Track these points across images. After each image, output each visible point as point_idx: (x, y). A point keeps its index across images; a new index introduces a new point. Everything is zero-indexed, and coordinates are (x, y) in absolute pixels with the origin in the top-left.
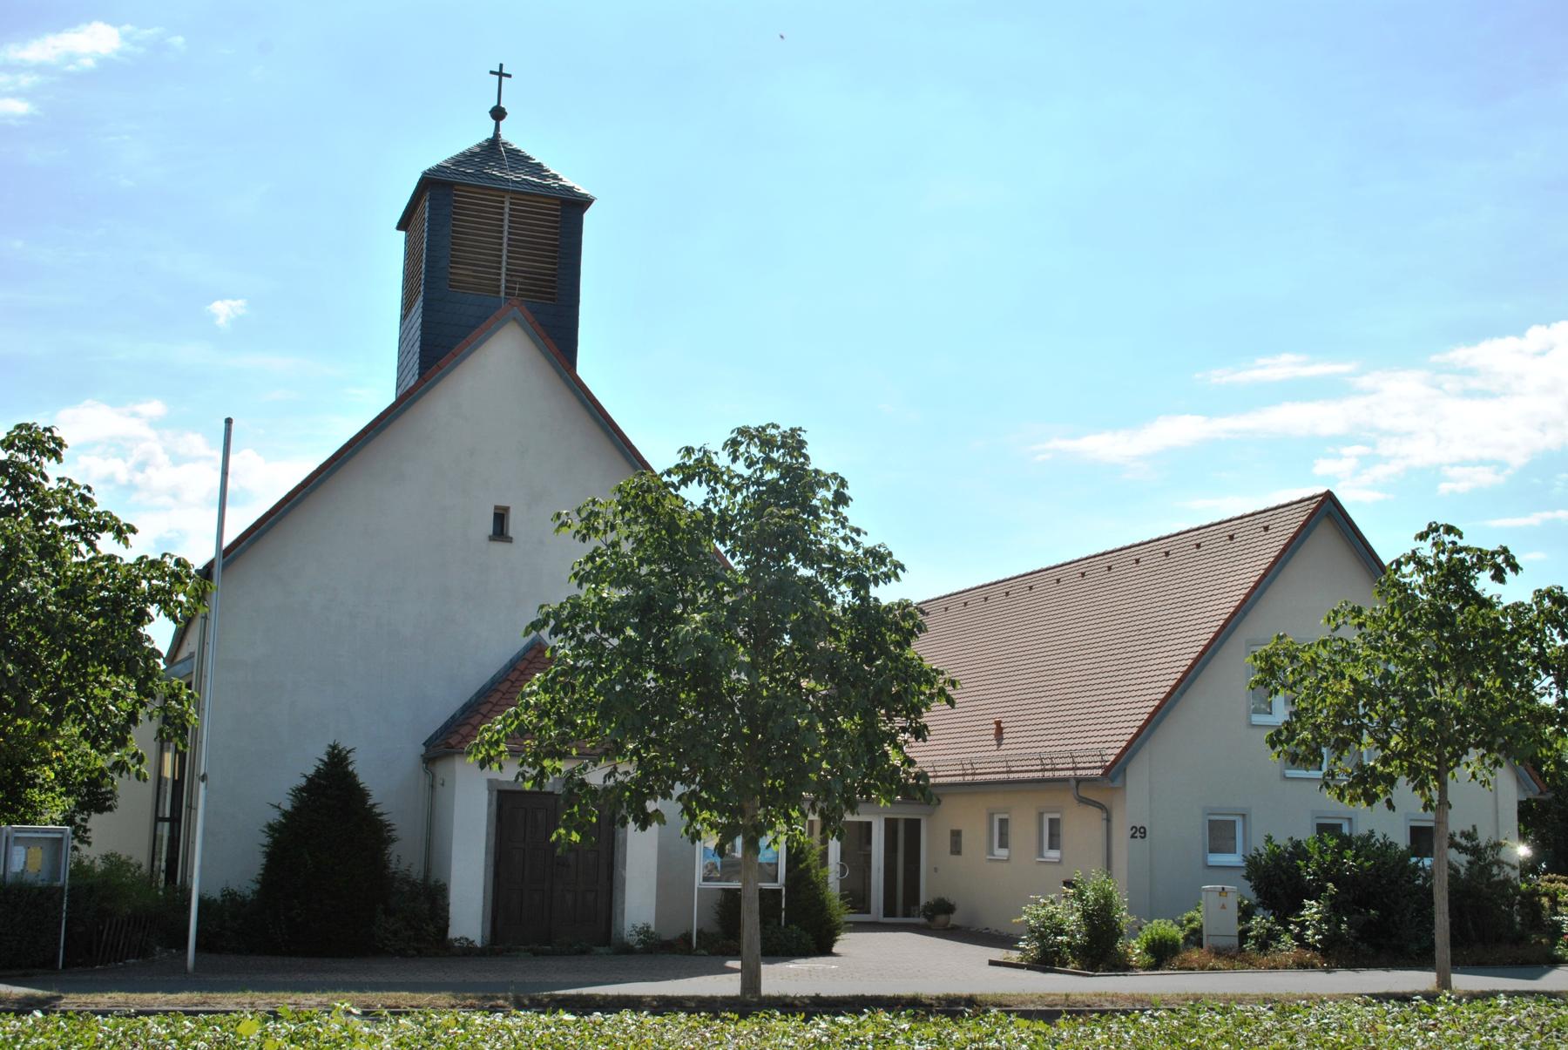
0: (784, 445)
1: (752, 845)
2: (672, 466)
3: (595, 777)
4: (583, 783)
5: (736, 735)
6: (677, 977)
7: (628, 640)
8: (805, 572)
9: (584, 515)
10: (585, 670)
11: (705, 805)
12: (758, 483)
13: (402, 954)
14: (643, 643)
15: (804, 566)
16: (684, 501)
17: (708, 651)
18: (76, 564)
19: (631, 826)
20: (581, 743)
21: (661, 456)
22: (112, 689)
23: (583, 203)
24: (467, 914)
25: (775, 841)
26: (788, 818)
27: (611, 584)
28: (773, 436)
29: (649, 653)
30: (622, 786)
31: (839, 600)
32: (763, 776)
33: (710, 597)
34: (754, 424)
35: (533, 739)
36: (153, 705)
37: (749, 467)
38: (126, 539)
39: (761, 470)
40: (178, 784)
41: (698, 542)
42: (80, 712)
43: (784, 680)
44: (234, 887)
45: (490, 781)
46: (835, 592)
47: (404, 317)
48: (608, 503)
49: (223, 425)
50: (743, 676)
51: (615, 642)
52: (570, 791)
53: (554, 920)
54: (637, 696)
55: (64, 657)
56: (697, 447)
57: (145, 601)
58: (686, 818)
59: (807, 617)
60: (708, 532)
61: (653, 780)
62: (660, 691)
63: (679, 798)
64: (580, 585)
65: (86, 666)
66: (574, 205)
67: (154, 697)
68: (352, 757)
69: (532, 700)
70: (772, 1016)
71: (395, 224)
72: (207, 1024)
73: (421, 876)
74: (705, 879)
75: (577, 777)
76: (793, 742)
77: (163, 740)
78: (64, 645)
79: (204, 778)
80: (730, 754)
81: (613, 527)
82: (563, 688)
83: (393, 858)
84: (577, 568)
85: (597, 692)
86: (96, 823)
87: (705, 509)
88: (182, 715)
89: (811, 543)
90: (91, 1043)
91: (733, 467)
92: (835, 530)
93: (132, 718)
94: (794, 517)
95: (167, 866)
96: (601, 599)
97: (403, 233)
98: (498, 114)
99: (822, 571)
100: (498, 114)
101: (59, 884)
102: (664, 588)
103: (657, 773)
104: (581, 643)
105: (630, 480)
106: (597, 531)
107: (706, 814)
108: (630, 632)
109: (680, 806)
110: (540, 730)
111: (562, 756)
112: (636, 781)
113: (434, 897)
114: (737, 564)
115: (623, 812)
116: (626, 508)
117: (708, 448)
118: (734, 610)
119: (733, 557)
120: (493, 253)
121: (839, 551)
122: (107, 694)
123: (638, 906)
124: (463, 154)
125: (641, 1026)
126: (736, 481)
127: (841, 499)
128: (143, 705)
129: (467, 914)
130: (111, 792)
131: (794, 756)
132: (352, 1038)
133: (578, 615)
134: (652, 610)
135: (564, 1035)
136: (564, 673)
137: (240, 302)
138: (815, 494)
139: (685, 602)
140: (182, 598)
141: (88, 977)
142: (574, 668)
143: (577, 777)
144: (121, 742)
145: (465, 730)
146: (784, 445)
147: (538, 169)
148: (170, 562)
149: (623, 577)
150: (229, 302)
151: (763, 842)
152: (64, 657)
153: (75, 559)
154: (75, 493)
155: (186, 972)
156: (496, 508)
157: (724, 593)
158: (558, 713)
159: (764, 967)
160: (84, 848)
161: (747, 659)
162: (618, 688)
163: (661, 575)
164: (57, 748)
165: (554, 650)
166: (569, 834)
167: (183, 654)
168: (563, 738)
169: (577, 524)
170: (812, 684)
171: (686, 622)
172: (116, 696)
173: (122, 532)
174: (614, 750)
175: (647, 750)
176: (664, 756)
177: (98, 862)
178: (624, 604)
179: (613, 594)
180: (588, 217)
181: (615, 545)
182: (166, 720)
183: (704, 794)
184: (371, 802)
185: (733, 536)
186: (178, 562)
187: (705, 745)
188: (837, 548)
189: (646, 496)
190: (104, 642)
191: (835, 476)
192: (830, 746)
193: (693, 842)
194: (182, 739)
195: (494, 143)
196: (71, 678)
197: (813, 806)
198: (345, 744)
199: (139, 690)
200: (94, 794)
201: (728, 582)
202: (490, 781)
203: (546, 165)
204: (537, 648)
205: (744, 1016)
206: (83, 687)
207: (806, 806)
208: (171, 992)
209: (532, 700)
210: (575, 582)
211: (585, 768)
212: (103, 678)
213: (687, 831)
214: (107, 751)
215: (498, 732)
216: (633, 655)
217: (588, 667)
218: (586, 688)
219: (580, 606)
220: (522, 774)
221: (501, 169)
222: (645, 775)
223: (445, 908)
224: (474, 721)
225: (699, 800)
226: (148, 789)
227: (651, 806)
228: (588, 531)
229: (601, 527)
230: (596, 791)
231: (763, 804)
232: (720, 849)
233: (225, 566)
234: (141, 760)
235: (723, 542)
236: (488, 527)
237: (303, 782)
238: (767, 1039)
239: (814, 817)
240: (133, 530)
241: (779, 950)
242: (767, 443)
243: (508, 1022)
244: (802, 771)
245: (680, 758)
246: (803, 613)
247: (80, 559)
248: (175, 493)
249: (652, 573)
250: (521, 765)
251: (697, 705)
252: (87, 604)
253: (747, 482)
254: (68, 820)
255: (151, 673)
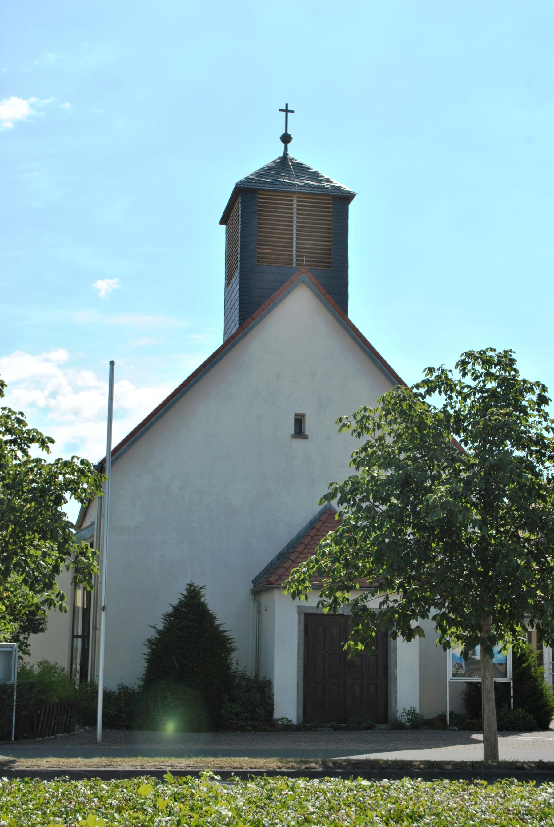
0: (499, 363)
1: (488, 651)
2: (419, 381)
3: (374, 603)
4: (365, 609)
5: (473, 572)
6: (437, 746)
7: (392, 505)
8: (519, 453)
9: (358, 418)
10: (363, 529)
11: (452, 623)
12: (481, 391)
13: (242, 729)
14: (404, 509)
15: (518, 449)
16: (429, 406)
17: (451, 513)
18: (16, 465)
19: (400, 638)
20: (362, 580)
21: (411, 375)
22: (41, 550)
23: (348, 197)
24: (287, 703)
25: (504, 648)
26: (513, 631)
27: (380, 467)
28: (491, 357)
29: (408, 516)
30: (392, 610)
31: (545, 472)
32: (494, 602)
33: (450, 474)
34: (477, 348)
35: (328, 577)
36: (69, 560)
37: (475, 380)
38: (47, 447)
39: (484, 381)
40: (86, 611)
41: (441, 434)
42: (20, 567)
43: (507, 532)
44: (126, 683)
45: (299, 607)
46: (533, 431)
47: (227, 285)
48: (376, 409)
49: (108, 366)
50: (477, 530)
51: (384, 508)
52: (356, 614)
53: (347, 703)
54: (401, 546)
55: (10, 529)
56: (436, 367)
57: (61, 489)
58: (439, 632)
59: (521, 486)
60: (447, 427)
61: (415, 605)
62: (417, 542)
63: (434, 618)
64: (357, 468)
65: (24, 535)
66: (342, 199)
67: (69, 554)
68: (203, 592)
69: (327, 550)
70: (512, 783)
71: (307, 416)
72: (117, 787)
73: (253, 674)
74: (454, 675)
75: (361, 604)
76: (515, 577)
77: (75, 584)
78: (10, 521)
79: (104, 609)
80: (469, 586)
81: (379, 427)
82: (349, 541)
83: (234, 662)
84: (355, 456)
85: (373, 544)
86: (34, 640)
87: (444, 411)
88: (89, 566)
89: (522, 432)
90: (42, 800)
91: (463, 380)
92: (540, 423)
93: (56, 569)
94: (509, 415)
95: (81, 668)
96: (373, 477)
97: (224, 227)
98: (286, 139)
99: (531, 453)
100: (286, 139)
101: (11, 682)
102: (417, 469)
103: (417, 601)
104: (360, 509)
105: (390, 392)
106: (368, 429)
107: (454, 629)
108: (394, 500)
109: (434, 624)
110: (333, 571)
111: (349, 589)
112: (402, 606)
113: (263, 689)
114: (469, 450)
115: (394, 629)
116: (388, 412)
117: (445, 367)
118: (468, 483)
119: (466, 445)
120: (286, 236)
121: (543, 438)
122: (39, 553)
123: (407, 694)
124: (263, 169)
125: (417, 789)
126: (465, 390)
127: (543, 400)
128: (63, 560)
129: (287, 703)
130: (43, 619)
131: (516, 588)
132: (216, 797)
133: (357, 489)
134: (409, 484)
135: (363, 796)
136: (349, 531)
137: (115, 280)
138: (523, 397)
139: (433, 478)
140: (85, 486)
141: (31, 746)
142: (355, 527)
143: (361, 604)
144: (49, 586)
145: (280, 571)
146: (499, 363)
147: (316, 176)
148: (77, 462)
149: (388, 462)
150: (107, 280)
151: (496, 648)
152: (10, 529)
153: (15, 462)
154: (13, 417)
155: (97, 743)
156: (296, 415)
157: (460, 471)
158: (346, 559)
159: (500, 740)
160: (26, 657)
161: (479, 517)
162: (387, 541)
163: (415, 460)
164: (6, 590)
165: (341, 514)
166: (356, 644)
167: (87, 523)
168: (350, 577)
169: (354, 425)
170: (527, 534)
171: (432, 492)
172: (45, 554)
173: (45, 442)
174: (386, 585)
175: (410, 584)
176: (422, 589)
177: (36, 667)
178: (389, 481)
179: (382, 474)
180: (353, 207)
181: (381, 439)
182: (77, 570)
183: (451, 615)
184: (217, 623)
185: (465, 430)
186: (82, 462)
187: (451, 580)
188: (541, 435)
189: (402, 403)
190: (36, 518)
191: (538, 383)
192: (543, 579)
193: (445, 650)
194: (89, 582)
195: (284, 159)
196: (15, 543)
197: (531, 622)
198: (198, 583)
199: (60, 550)
200: (32, 620)
201: (463, 463)
202: (299, 607)
203: (321, 173)
204: (328, 513)
205: (491, 782)
206: (23, 549)
207: (526, 622)
208: (87, 757)
209: (327, 550)
210: (354, 466)
211: (366, 598)
212: (36, 543)
213: (440, 642)
214: (40, 592)
215: (304, 573)
216: (397, 516)
217: (366, 526)
218: (365, 541)
219: (359, 483)
220: (321, 603)
221: (290, 178)
222: (409, 602)
223: (271, 697)
224: (287, 565)
225: (449, 620)
226: (67, 617)
227: (414, 624)
228: (362, 429)
229: (371, 427)
230: (374, 614)
231: (495, 621)
232: (465, 654)
233: (113, 462)
234: (62, 598)
235: (458, 434)
236: (291, 428)
237: (171, 610)
238: (508, 800)
239: (534, 630)
240: (52, 441)
241: (511, 726)
242: (487, 362)
243: (323, 786)
244: (522, 597)
245: (433, 589)
246: (519, 483)
247: (18, 462)
248: (76, 412)
249: (408, 458)
250: (321, 596)
251: (444, 551)
252: (23, 492)
253: (474, 390)
254: (15, 639)
255: (67, 539)
